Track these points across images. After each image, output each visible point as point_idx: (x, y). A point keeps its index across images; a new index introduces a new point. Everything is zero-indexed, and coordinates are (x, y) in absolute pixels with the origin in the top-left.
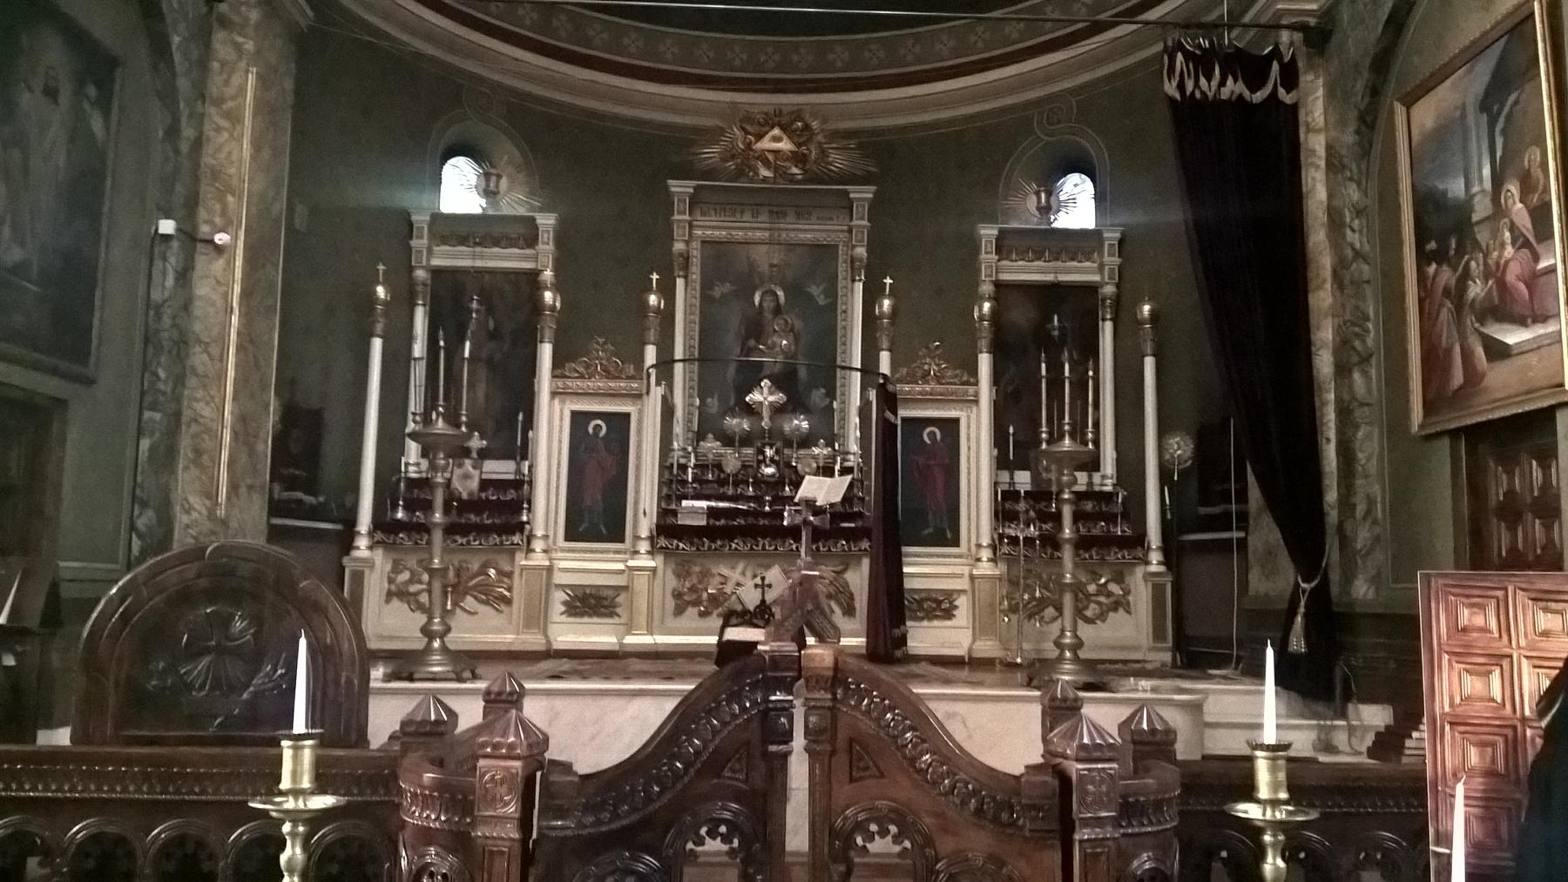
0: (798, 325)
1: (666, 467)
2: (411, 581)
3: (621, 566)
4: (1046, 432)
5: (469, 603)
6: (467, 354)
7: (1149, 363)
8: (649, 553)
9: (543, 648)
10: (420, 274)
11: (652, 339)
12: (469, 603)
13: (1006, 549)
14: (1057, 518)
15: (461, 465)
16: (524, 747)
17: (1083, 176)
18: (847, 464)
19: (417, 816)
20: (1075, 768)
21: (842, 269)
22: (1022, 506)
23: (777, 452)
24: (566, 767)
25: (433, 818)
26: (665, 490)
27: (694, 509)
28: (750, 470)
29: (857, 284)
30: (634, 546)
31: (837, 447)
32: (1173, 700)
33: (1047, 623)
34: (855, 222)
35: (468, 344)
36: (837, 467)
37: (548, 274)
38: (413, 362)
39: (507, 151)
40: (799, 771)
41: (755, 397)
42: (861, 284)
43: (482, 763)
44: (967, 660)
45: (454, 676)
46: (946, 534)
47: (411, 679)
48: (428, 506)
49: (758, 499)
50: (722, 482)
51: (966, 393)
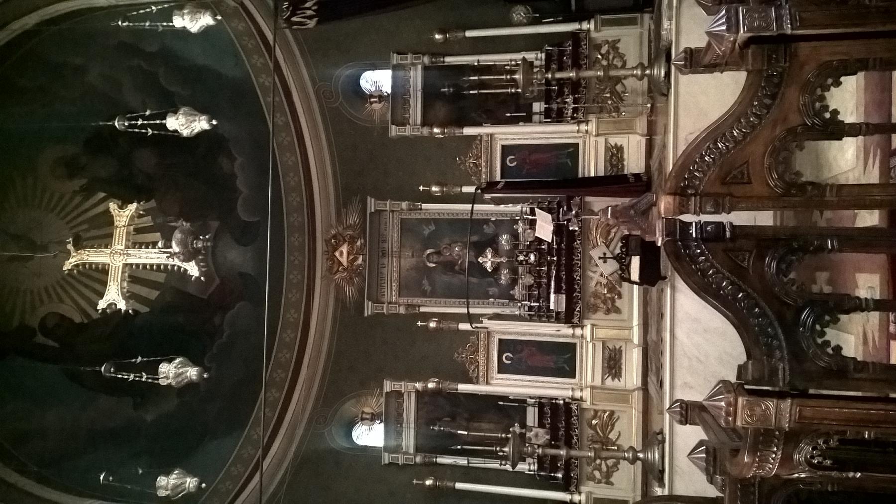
0: (447, 241)
1: (530, 318)
2: (600, 470)
3: (590, 345)
4: (511, 90)
5: (613, 436)
6: (466, 433)
7: (469, 34)
8: (582, 329)
9: (641, 393)
10: (418, 459)
11: (456, 326)
12: (613, 436)
13: (580, 115)
14: (561, 82)
15: (530, 439)
16: (730, 395)
17: (362, 77)
18: (528, 212)
19: (772, 468)
20: (743, 34)
21: (415, 215)
22: (555, 106)
23: (521, 253)
24: (741, 369)
25: (775, 455)
26: (544, 319)
27: (558, 302)
28: (532, 269)
29: (423, 207)
30: (578, 337)
31: (519, 218)
32: (676, 7)
33: (626, 89)
34: (388, 209)
35: (459, 432)
36: (530, 217)
37: (419, 386)
38: (470, 465)
39: (350, 408)
40: (740, 218)
41: (489, 266)
42: (423, 204)
43: (739, 423)
44: (648, 137)
45: (661, 445)
46: (571, 151)
47: (662, 472)
48: (555, 458)
49: (549, 265)
50: (539, 286)
51: (487, 142)
